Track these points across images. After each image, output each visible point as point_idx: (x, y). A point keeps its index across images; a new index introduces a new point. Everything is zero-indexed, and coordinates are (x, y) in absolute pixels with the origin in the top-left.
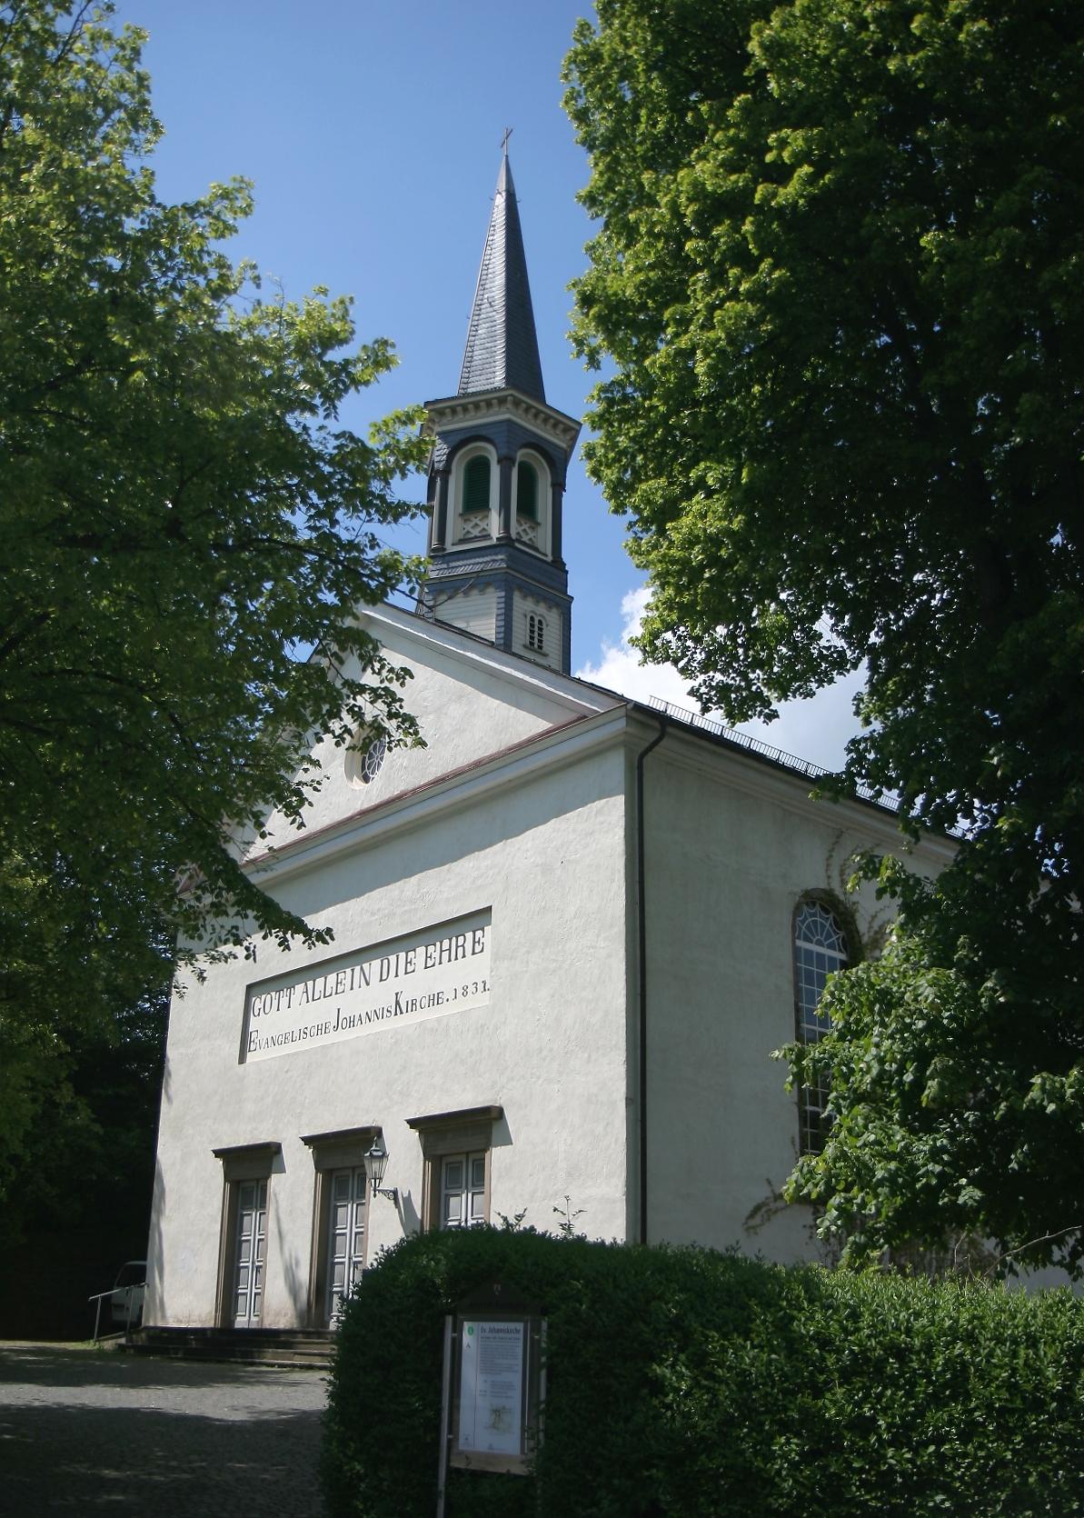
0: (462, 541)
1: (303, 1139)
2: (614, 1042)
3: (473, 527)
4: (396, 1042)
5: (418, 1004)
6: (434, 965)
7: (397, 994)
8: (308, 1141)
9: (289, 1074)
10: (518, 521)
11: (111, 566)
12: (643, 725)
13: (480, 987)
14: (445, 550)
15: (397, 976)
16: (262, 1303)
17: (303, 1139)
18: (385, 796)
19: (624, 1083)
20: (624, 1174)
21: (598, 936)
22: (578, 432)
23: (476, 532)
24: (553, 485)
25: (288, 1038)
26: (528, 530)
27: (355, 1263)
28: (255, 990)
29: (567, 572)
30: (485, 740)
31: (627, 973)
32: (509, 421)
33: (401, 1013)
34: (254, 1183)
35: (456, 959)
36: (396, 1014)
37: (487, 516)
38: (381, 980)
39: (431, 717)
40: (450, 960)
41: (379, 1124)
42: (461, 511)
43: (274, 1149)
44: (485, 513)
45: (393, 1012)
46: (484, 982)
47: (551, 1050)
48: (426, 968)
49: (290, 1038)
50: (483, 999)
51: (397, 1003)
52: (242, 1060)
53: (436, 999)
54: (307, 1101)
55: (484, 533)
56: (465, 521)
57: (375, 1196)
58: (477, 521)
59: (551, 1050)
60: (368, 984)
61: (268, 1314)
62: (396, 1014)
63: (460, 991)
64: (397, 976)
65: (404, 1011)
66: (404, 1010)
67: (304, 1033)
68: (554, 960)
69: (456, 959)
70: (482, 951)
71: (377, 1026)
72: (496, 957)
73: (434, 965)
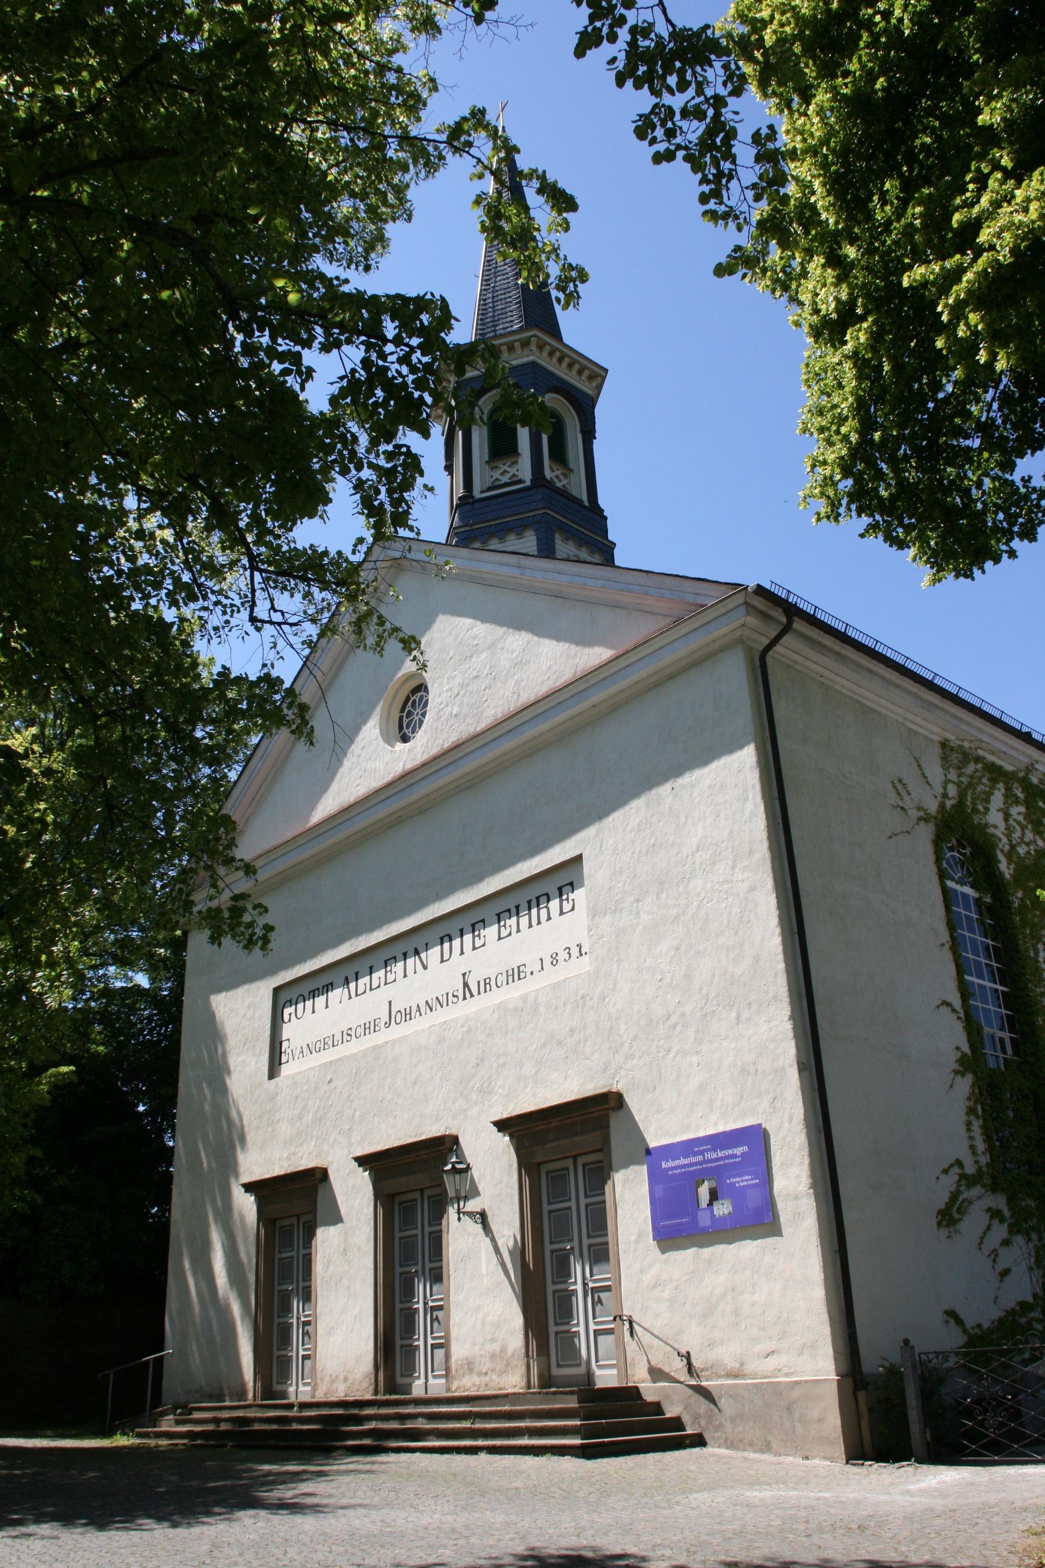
0: (490, 489)
1: (356, 1159)
2: (771, 995)
3: (501, 474)
4: (469, 1031)
5: (493, 983)
6: (510, 934)
7: (464, 975)
8: (363, 1161)
9: (333, 1085)
10: (551, 467)
11: (88, 842)
12: (766, 617)
13: (575, 952)
14: (473, 497)
15: (462, 953)
16: (314, 1368)
17: (356, 1159)
18: (434, 751)
19: (792, 1044)
20: (807, 1160)
21: (733, 867)
22: (604, 378)
23: (505, 479)
24: (582, 431)
25: (327, 1043)
26: (562, 477)
27: (433, 1308)
28: (284, 997)
29: (606, 518)
30: (555, 668)
31: (779, 908)
32: (533, 364)
33: (472, 996)
34: (294, 1221)
35: (539, 923)
36: (465, 998)
37: (517, 462)
38: (442, 961)
39: (484, 655)
40: (530, 926)
41: (454, 1132)
42: (487, 459)
43: (318, 1175)
44: (514, 459)
45: (461, 997)
46: (580, 946)
47: (683, 1015)
48: (500, 938)
49: (330, 1043)
50: (583, 966)
51: (466, 985)
52: (273, 1073)
53: (516, 974)
54: (357, 1114)
55: (515, 479)
56: (492, 469)
57: (459, 1219)
58: (505, 467)
59: (683, 1015)
60: (425, 967)
61: (322, 1379)
62: (465, 998)
63: (547, 961)
64: (462, 953)
65: (445, 1004)
66: (475, 992)
67: (348, 1034)
68: (675, 906)
69: (539, 923)
70: (573, 909)
71: (441, 1016)
72: (594, 913)
73: (510, 934)
